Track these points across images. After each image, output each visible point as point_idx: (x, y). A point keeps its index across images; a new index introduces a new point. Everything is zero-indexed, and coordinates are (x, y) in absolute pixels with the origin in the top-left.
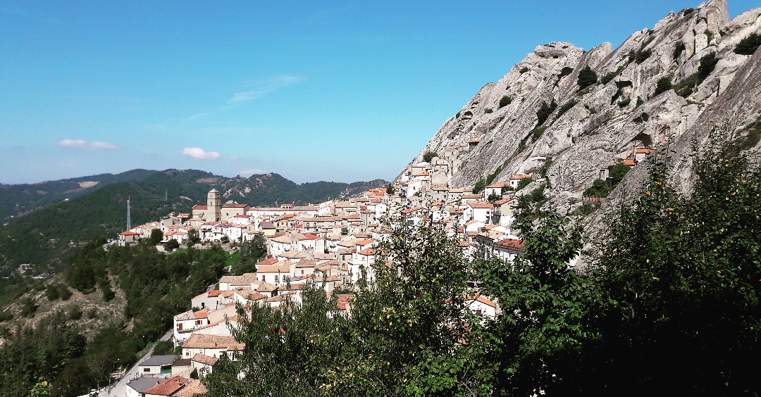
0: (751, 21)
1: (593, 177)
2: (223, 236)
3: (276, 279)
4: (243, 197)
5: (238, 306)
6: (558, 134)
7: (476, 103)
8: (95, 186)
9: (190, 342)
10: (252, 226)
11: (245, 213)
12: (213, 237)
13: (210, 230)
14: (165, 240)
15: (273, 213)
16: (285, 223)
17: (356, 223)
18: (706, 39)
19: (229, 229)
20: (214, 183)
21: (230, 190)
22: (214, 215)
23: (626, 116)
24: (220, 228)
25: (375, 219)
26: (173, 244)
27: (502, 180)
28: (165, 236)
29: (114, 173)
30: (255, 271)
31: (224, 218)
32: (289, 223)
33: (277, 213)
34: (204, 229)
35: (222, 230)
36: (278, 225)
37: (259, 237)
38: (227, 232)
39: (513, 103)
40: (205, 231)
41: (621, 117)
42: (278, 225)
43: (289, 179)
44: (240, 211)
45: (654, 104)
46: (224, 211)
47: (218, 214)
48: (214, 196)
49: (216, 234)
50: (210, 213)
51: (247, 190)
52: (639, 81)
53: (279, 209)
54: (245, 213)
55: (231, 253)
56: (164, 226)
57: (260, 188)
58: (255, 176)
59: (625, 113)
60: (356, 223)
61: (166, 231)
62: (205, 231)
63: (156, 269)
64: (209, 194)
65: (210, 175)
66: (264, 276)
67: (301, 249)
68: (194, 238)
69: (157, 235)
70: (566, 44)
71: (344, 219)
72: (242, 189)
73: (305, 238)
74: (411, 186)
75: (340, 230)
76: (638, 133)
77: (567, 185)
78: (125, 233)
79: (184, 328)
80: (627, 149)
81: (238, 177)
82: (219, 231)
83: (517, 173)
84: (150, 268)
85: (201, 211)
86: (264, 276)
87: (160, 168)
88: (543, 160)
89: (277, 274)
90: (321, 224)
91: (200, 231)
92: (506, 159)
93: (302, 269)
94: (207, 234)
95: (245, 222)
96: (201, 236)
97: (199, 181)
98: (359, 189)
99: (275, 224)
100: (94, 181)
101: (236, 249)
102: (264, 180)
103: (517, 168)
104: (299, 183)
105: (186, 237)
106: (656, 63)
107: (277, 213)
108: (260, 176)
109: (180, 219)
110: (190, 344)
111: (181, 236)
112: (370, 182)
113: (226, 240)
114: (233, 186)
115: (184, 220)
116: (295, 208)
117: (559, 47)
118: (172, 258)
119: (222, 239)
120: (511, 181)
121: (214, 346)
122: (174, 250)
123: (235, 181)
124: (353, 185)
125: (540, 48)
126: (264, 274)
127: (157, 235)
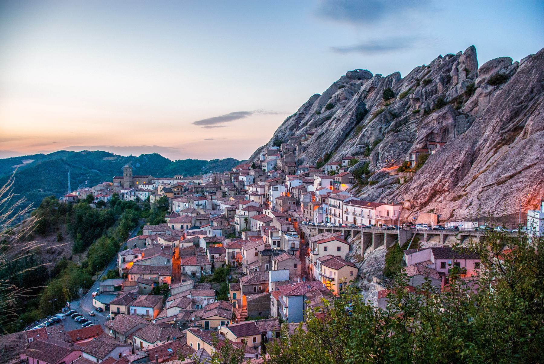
1: (328, 275)
8: (33, 163)
9: (132, 270)
15: (169, 182)
18: (465, 74)
20: (115, 160)
27: (336, 158)
29: (221, 158)
30: (165, 222)
33: (172, 181)
39: (335, 108)
41: (414, 121)
50: (126, 181)
53: (173, 179)
59: (417, 119)
65: (112, 155)
66: (173, 226)
69: (90, 198)
77: (384, 164)
78: (294, 176)
79: (126, 260)
86: (173, 226)
88: (364, 147)
89: (182, 224)
93: (200, 221)
97: (105, 159)
100: (32, 159)
103: (347, 152)
106: (434, 88)
110: (132, 271)
113: (138, 199)
120: (343, 161)
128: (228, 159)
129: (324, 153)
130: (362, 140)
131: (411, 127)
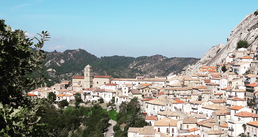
2: (99, 98)
3: (167, 131)
4: (59, 67)
10: (119, 91)
11: (110, 82)
12: (93, 98)
13: (89, 93)
14: (57, 100)
15: (131, 82)
16: (147, 91)
17: (206, 92)
19: (104, 93)
21: (49, 61)
22: (89, 83)
24: (97, 93)
25: (219, 89)
26: (64, 103)
28: (57, 98)
31: (95, 85)
32: (150, 91)
34: (85, 93)
35: (98, 94)
36: (143, 91)
37: (135, 100)
38: (102, 95)
40: (85, 94)
42: (143, 91)
43: (92, 54)
44: (107, 81)
46: (95, 80)
47: (91, 82)
48: (89, 70)
49: (93, 96)
51: (62, 61)
53: (134, 79)
54: (110, 82)
55: (108, 110)
56: (56, 89)
57: (72, 60)
58: (67, 52)
60: (206, 92)
61: (57, 94)
62: (85, 94)
63: (58, 121)
64: (85, 69)
66: (159, 129)
67: (174, 110)
69: (52, 96)
71: (194, 89)
72: (59, 61)
73: (176, 102)
74: (242, 66)
75: (197, 97)
81: (55, 51)
82: (96, 94)
84: (55, 120)
85: (78, 80)
86: (159, 129)
87: (110, 55)
89: (168, 127)
90: (178, 92)
91: (82, 94)
94: (87, 97)
95: (113, 88)
96: (83, 97)
98: (143, 62)
99: (141, 91)
101: (112, 108)
102: (73, 54)
104: (99, 56)
105: (73, 98)
107: (134, 83)
109: (64, 86)
111: (69, 97)
112: (151, 57)
114: (52, 58)
115: (67, 86)
116: (146, 79)
118: (69, 113)
119: (98, 100)
122: (66, 107)
123: (53, 55)
124: (138, 59)
126: (159, 127)
127: (52, 96)
128: (157, 56)
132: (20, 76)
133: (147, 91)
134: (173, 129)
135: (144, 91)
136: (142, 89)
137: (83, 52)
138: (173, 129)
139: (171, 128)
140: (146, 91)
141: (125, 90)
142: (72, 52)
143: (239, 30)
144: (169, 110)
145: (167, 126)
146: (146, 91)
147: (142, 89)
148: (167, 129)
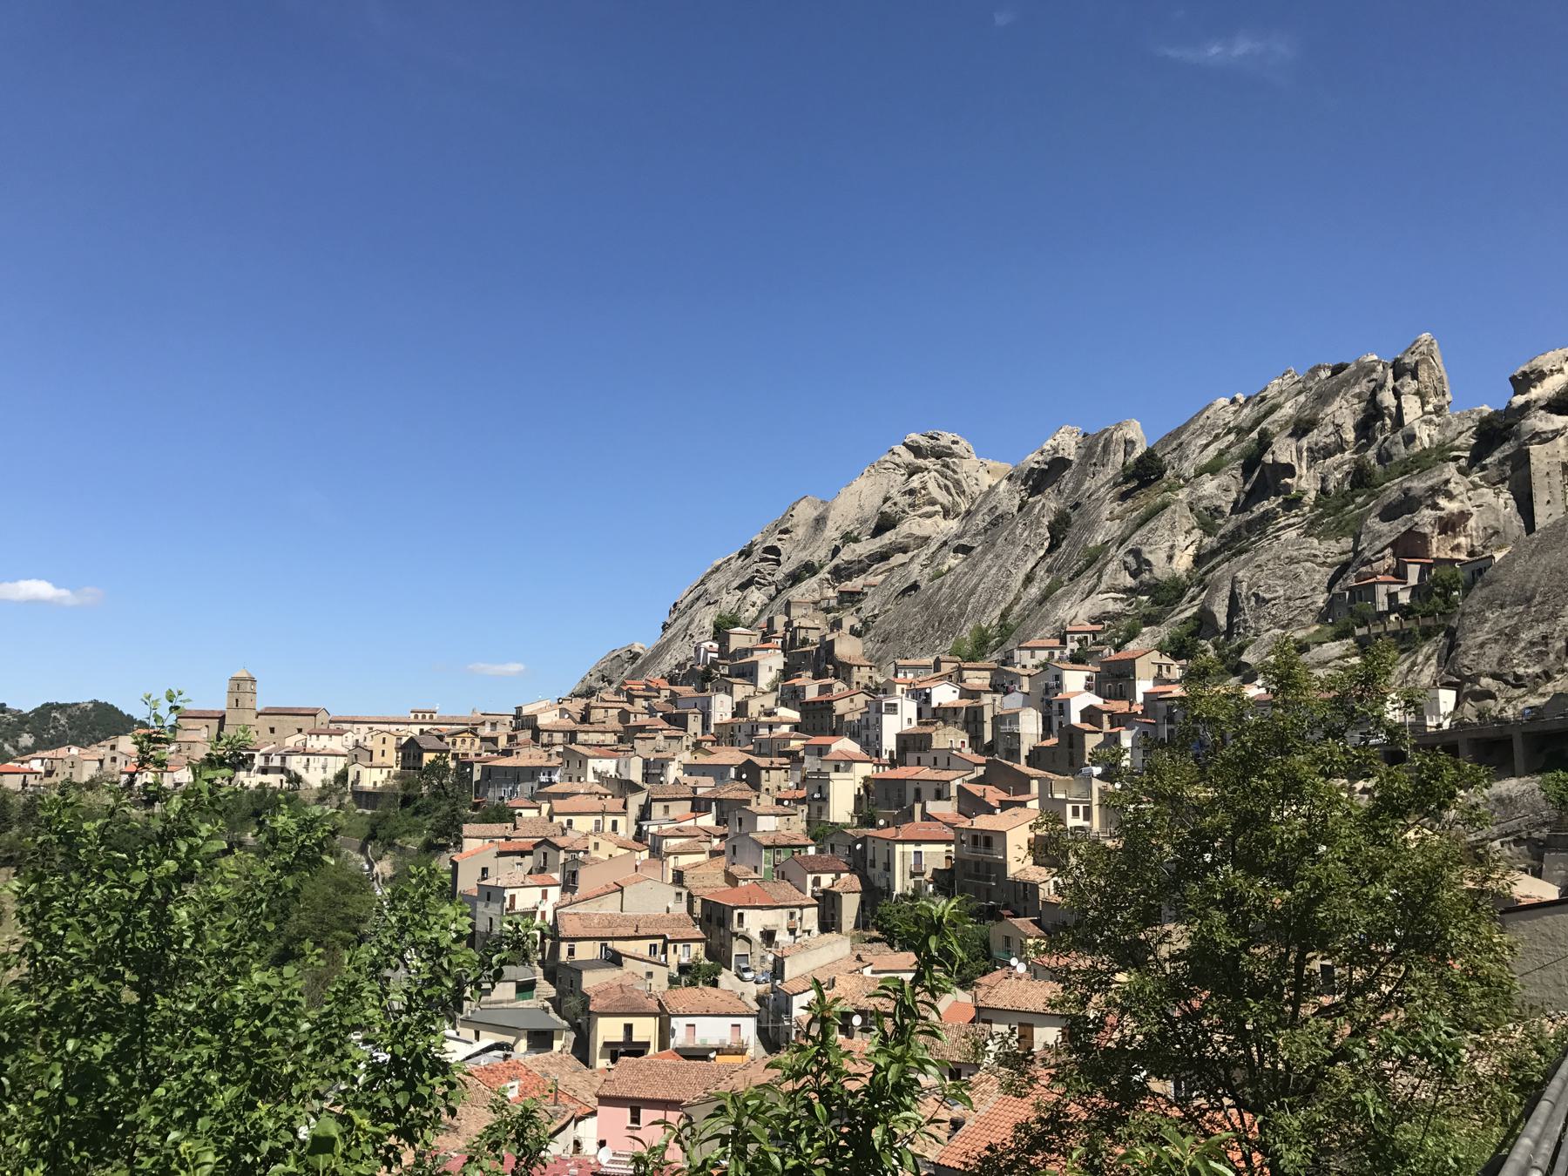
0: (1557, 367)
5: (363, 920)
6: (1150, 552)
7: (786, 531)
16: (468, 741)
18: (1419, 404)
23: (1300, 519)
36: (454, 744)
45: (1430, 483)
52: (1304, 464)
58: (48, 708)
68: (1337, 541)
70: (957, 438)
76: (1403, 530)
80: (1383, 558)
83: (1074, 622)
89: (600, 818)
92: (1003, 606)
102: (70, 717)
103: (1073, 613)
108: (61, 708)
117: (946, 439)
121: (632, 932)
125: (914, 437)
129: (970, 625)
130: (1116, 579)
131: (1283, 538)
132: (849, 620)
133: (468, 741)
134: (615, 823)
135: (459, 741)
136: (451, 735)
137: (47, 704)
138: (615, 823)
139: (609, 819)
140: (464, 741)
141: (383, 747)
142: (65, 711)
143: (698, 599)
144: (574, 779)
145: (595, 814)
146: (464, 741)
147: (451, 735)
148: (597, 822)
